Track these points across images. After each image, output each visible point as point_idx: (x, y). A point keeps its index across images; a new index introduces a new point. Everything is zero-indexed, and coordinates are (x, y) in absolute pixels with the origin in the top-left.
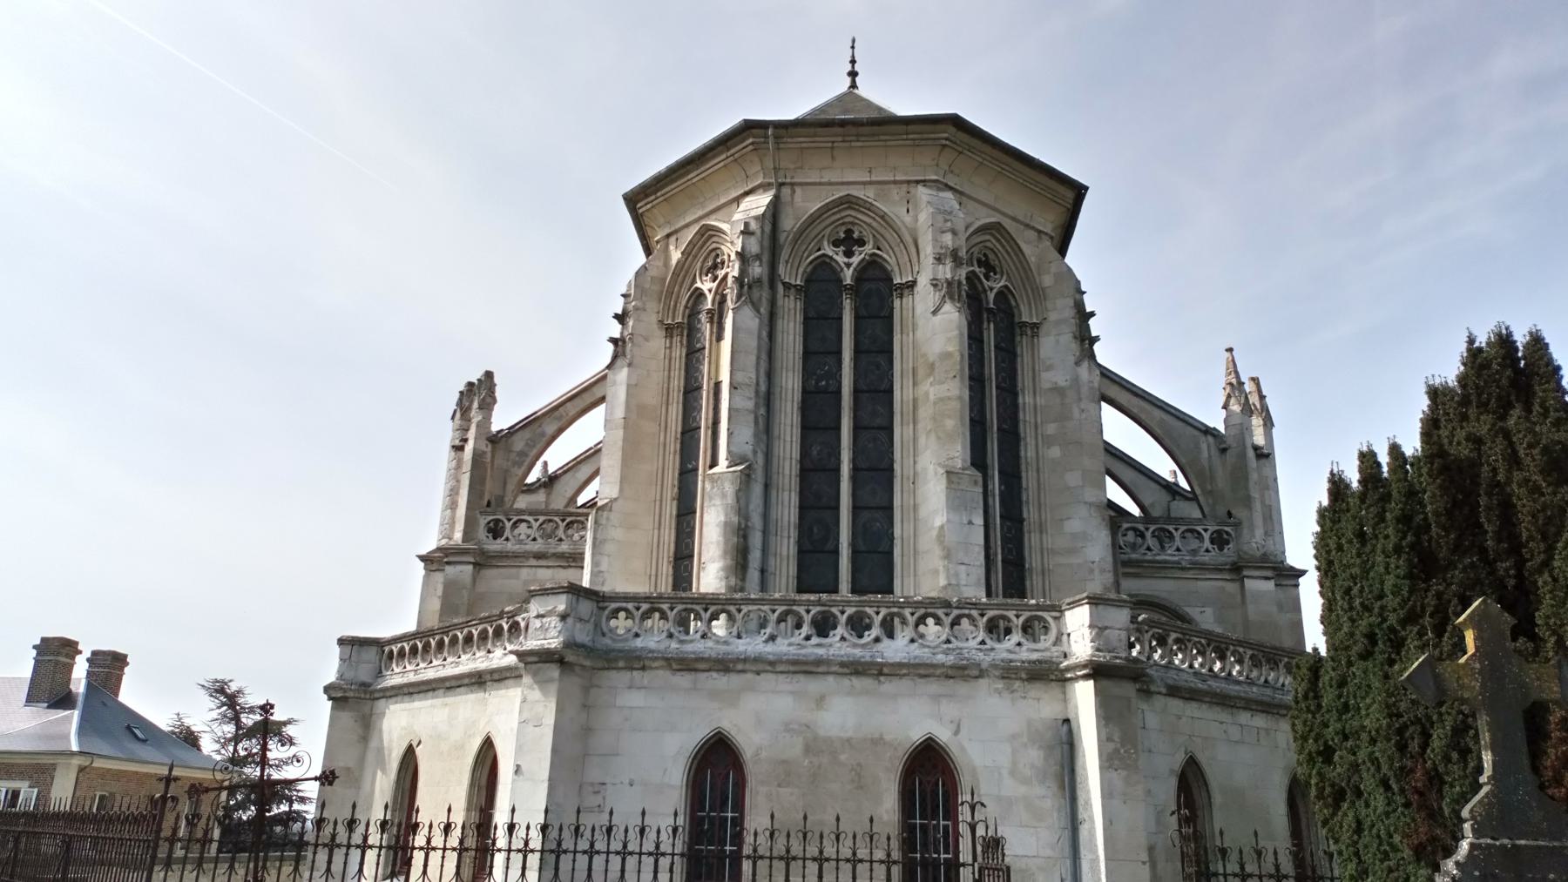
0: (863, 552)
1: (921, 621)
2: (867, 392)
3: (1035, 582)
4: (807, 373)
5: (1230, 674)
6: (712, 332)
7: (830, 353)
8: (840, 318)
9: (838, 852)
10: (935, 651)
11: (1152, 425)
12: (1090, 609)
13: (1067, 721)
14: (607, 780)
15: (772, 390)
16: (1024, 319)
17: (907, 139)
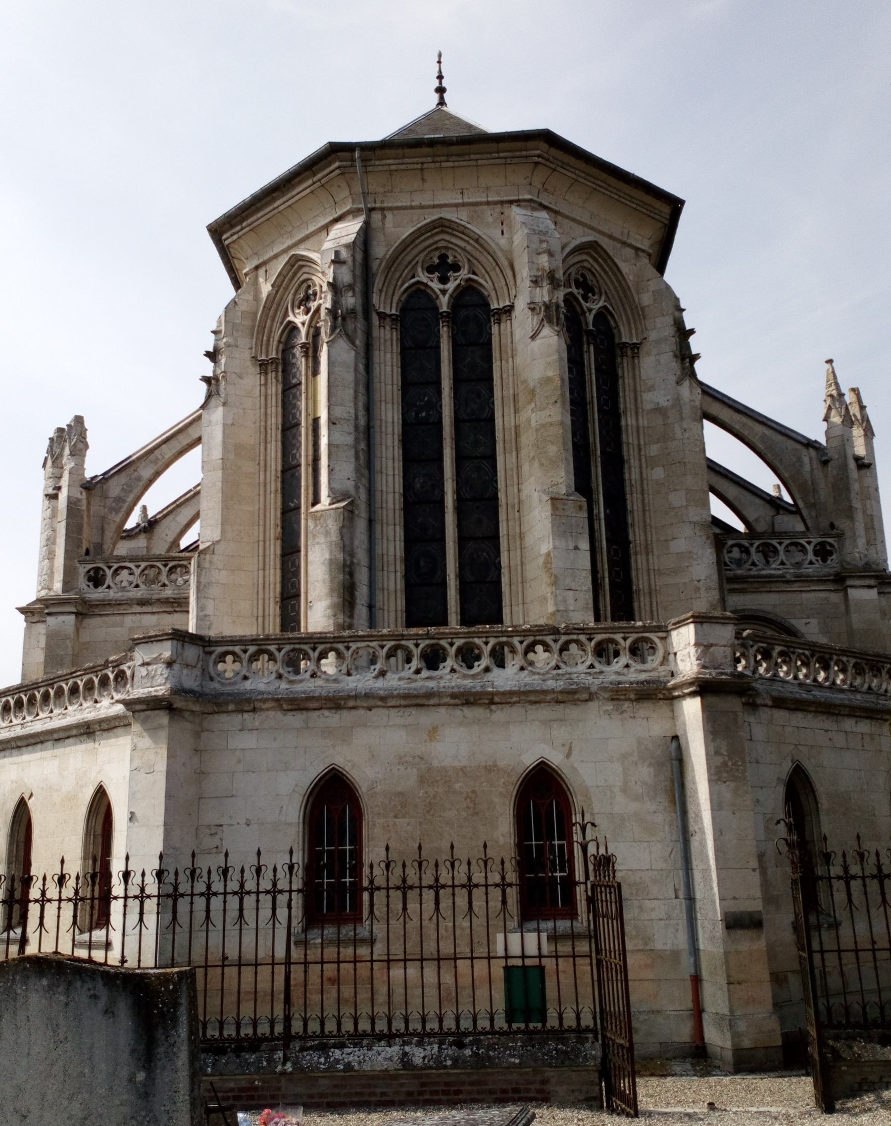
1: (530, 648)
3: (642, 604)
5: (834, 683)
8: (438, 348)
10: (546, 677)
13: (676, 738)
15: (371, 424)
16: (624, 340)
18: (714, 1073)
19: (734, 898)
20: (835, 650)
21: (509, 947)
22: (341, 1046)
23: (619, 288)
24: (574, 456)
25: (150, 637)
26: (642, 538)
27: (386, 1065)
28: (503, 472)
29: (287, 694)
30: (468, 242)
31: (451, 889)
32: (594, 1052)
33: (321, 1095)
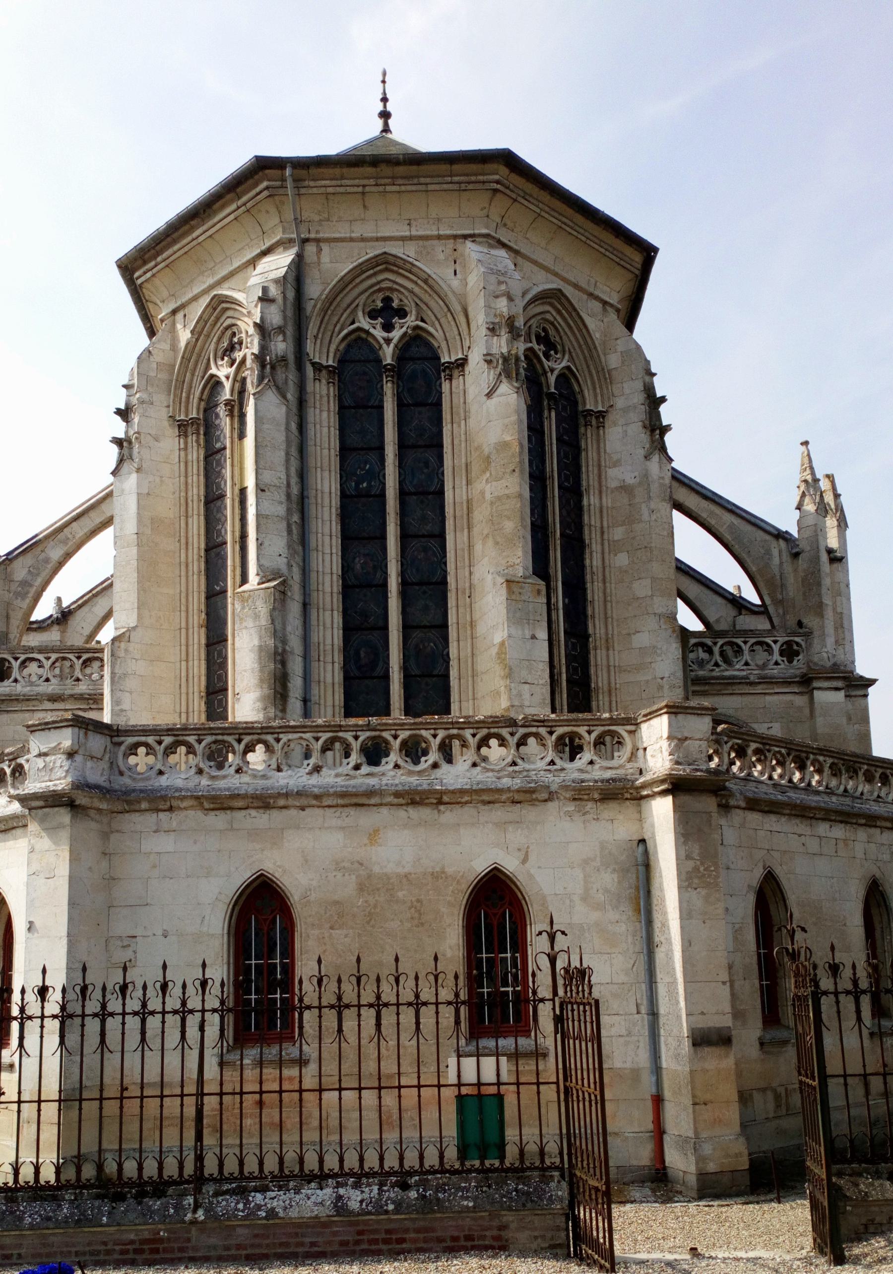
0: (416, 676)
1: (484, 742)
2: (415, 494)
3: (601, 703)
4: (345, 474)
5: (809, 784)
6: (232, 429)
7: (370, 449)
8: (381, 407)
9: (398, 995)
10: (501, 774)
11: (721, 530)
12: (669, 718)
13: (643, 841)
14: (139, 932)
15: (305, 493)
16: (588, 407)
17: (451, 183)
18: (676, 1199)
19: (703, 1013)
20: (813, 748)
21: (462, 1074)
22: (264, 1190)
23: (584, 347)
24: (532, 537)
25: (47, 723)
26: (603, 631)
27: (317, 1211)
28: (453, 552)
29: (208, 791)
30: (416, 283)
31: (395, 1007)
32: (560, 1193)
33: (239, 1247)
